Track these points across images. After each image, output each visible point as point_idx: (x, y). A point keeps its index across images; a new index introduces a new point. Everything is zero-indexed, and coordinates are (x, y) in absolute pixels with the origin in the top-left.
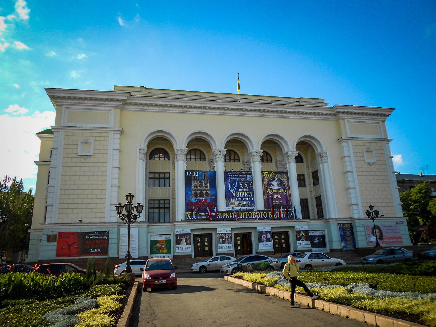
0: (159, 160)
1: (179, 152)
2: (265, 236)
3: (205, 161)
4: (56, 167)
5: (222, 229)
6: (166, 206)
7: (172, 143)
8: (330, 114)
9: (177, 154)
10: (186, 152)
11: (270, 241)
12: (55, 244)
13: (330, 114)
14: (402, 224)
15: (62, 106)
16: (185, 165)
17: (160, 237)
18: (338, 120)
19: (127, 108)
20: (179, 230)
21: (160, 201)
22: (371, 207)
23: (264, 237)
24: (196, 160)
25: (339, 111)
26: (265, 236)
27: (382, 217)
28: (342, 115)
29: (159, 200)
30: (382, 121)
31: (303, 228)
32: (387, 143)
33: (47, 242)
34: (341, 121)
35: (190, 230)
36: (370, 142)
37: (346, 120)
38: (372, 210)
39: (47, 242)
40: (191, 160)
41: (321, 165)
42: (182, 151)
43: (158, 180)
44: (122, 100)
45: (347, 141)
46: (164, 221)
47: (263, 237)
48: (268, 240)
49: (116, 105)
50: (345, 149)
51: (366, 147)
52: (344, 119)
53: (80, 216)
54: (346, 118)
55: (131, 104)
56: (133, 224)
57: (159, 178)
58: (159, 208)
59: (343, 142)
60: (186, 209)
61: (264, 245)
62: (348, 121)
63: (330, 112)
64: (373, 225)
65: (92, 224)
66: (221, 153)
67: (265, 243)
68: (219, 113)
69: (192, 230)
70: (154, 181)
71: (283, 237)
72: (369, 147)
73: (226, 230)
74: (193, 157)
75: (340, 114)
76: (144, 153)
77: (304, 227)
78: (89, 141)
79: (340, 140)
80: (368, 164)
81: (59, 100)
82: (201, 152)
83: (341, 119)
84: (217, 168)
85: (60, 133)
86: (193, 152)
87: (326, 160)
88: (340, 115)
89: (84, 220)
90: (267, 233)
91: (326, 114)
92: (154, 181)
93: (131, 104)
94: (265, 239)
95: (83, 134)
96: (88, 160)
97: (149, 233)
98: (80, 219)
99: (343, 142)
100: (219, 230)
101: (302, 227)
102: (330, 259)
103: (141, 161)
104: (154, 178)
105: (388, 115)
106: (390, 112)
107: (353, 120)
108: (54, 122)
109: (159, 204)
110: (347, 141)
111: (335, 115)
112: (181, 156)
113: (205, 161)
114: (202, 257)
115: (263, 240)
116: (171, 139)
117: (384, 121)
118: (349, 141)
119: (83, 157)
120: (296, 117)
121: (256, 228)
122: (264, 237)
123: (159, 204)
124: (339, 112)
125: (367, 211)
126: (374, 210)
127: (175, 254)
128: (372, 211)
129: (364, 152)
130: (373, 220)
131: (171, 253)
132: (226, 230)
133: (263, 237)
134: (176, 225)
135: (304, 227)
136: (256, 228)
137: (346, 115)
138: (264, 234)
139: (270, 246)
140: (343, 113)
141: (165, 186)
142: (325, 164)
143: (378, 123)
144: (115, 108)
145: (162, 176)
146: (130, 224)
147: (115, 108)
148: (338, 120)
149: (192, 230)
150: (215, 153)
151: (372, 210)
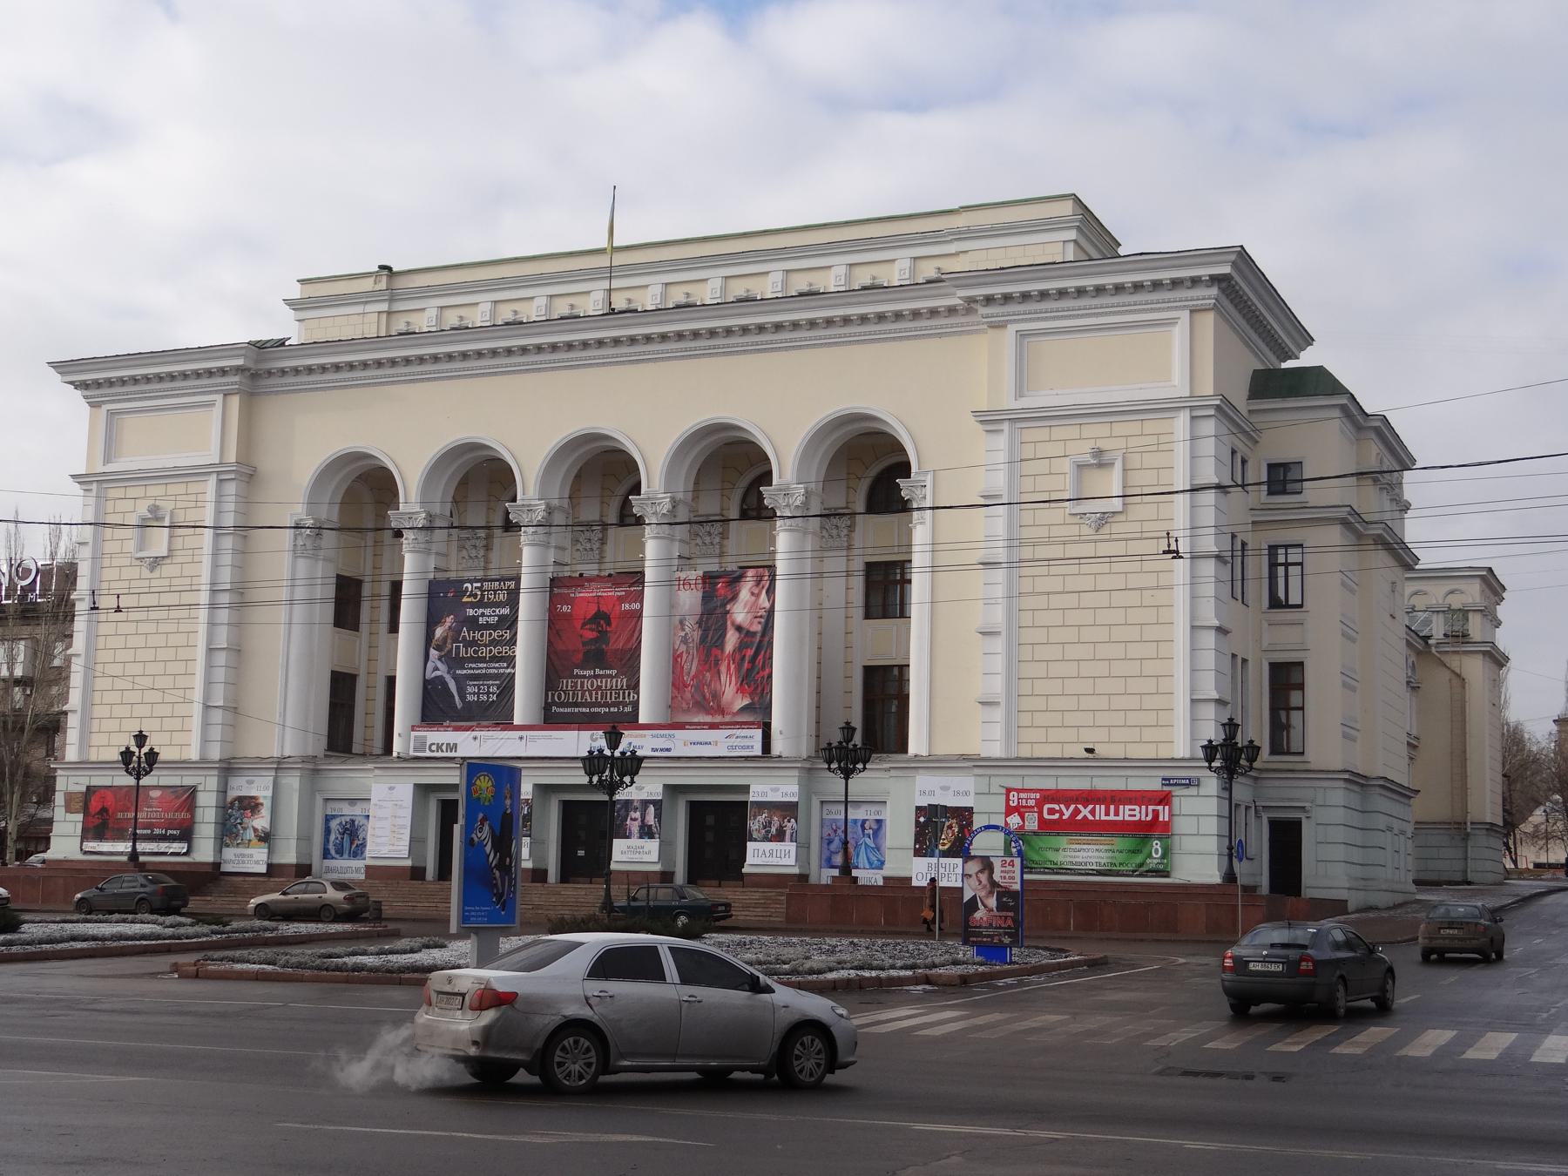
2: (637, 815)
11: (651, 836)
12: (522, 797)
14: (1193, 791)
22: (141, 738)
23: (635, 820)
26: (637, 815)
31: (644, 790)
35: (660, 789)
38: (140, 746)
47: (631, 819)
48: (646, 832)
51: (1091, 444)
53: (1090, 737)
61: (628, 847)
64: (850, 781)
67: (635, 842)
73: (779, 793)
89: (1101, 751)
90: (645, 804)
94: (635, 827)
97: (317, 793)
98: (1091, 746)
102: (853, 1063)
107: (238, 966)
115: (630, 830)
122: (635, 820)
125: (128, 748)
126: (145, 750)
128: (140, 752)
132: (779, 793)
133: (631, 819)
138: (636, 810)
139: (650, 852)
151: (140, 746)
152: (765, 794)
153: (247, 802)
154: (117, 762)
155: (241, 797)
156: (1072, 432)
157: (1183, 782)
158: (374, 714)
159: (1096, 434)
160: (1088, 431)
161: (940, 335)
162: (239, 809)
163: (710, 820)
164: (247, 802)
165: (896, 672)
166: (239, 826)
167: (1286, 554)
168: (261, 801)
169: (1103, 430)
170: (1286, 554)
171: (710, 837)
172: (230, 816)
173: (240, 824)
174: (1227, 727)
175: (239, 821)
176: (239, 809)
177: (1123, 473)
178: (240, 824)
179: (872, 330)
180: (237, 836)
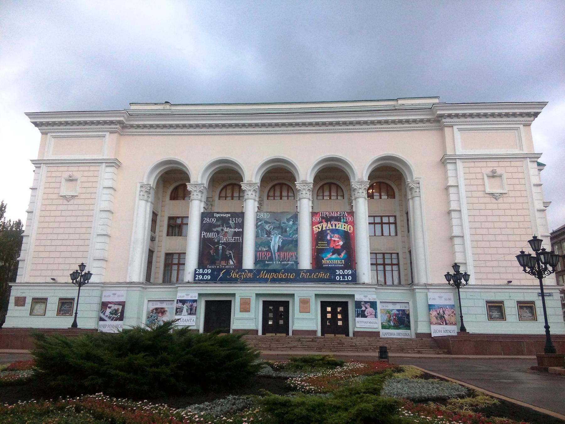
0: (330, 198)
1: (194, 189)
3: (394, 198)
4: (33, 212)
5: (184, 294)
6: (395, 261)
7: (348, 175)
8: (429, 121)
9: (355, 189)
10: (368, 186)
13: (429, 121)
15: (47, 134)
16: (311, 204)
17: (160, 304)
18: (441, 129)
19: (127, 132)
20: (182, 294)
21: (385, 254)
24: (281, 199)
25: (441, 114)
27: (510, 284)
28: (448, 120)
29: (384, 254)
30: (525, 125)
32: (106, 166)
33: (15, 306)
34: (447, 130)
35: (197, 295)
36: (510, 160)
37: (455, 127)
39: (15, 306)
40: (240, 199)
41: (410, 201)
42: (197, 186)
43: (380, 225)
44: (120, 122)
45: (454, 161)
46: (391, 284)
49: (111, 128)
50: (450, 173)
51: (491, 169)
52: (452, 126)
53: (55, 274)
54: (457, 125)
55: (132, 126)
56: (465, 287)
57: (382, 223)
58: (384, 265)
59: (448, 163)
60: (150, 267)
62: (460, 130)
63: (428, 117)
65: (61, 285)
66: (363, 186)
68: (252, 131)
69: (200, 295)
70: (389, 226)
71: (329, 309)
72: (495, 168)
73: (190, 296)
74: (327, 193)
75: (445, 118)
76: (309, 190)
77: (369, 296)
78: (74, 178)
79: (445, 161)
80: (491, 196)
81: (43, 127)
82: (388, 186)
83: (445, 127)
84: (300, 209)
85: (41, 168)
86: (326, 188)
87: (417, 193)
88: (444, 120)
91: (422, 121)
92: (389, 226)
93: (132, 126)
95: (499, 164)
96: (72, 202)
99: (448, 163)
100: (358, 298)
101: (187, 295)
103: (143, 203)
104: (374, 223)
105: (536, 115)
106: (539, 108)
108: (37, 155)
109: (384, 258)
110: (454, 161)
111: (439, 121)
112: (195, 193)
113: (394, 198)
114: (275, 334)
116: (348, 170)
117: (530, 125)
118: (458, 161)
119: (66, 198)
120: (419, 127)
121: (353, 296)
123: (384, 258)
124: (442, 116)
127: (356, 330)
129: (485, 177)
130: (80, 286)
131: (410, 329)
134: (417, 291)
135: (369, 296)
136: (353, 296)
137: (455, 120)
140: (450, 116)
141: (375, 235)
142: (417, 199)
143: (517, 129)
144: (111, 132)
145: (385, 220)
146: (460, 287)
147: (110, 133)
148: (441, 129)
149: (200, 295)
150: (410, 185)
152: (184, 296)
153: (159, 310)
154: (546, 295)
155: (156, 308)
156: (483, 164)
157: (547, 294)
158: (159, 268)
159: (493, 165)
160: (490, 164)
161: (133, 135)
162: (156, 313)
163: (281, 309)
164: (159, 310)
165: (176, 256)
166: (156, 320)
167: (389, 223)
168: (166, 309)
169: (495, 164)
170: (389, 223)
171: (329, 316)
172: (152, 316)
173: (157, 319)
174: (447, 276)
175: (156, 318)
176: (156, 313)
177: (484, 183)
178: (157, 319)
179: (114, 127)
180: (155, 324)
